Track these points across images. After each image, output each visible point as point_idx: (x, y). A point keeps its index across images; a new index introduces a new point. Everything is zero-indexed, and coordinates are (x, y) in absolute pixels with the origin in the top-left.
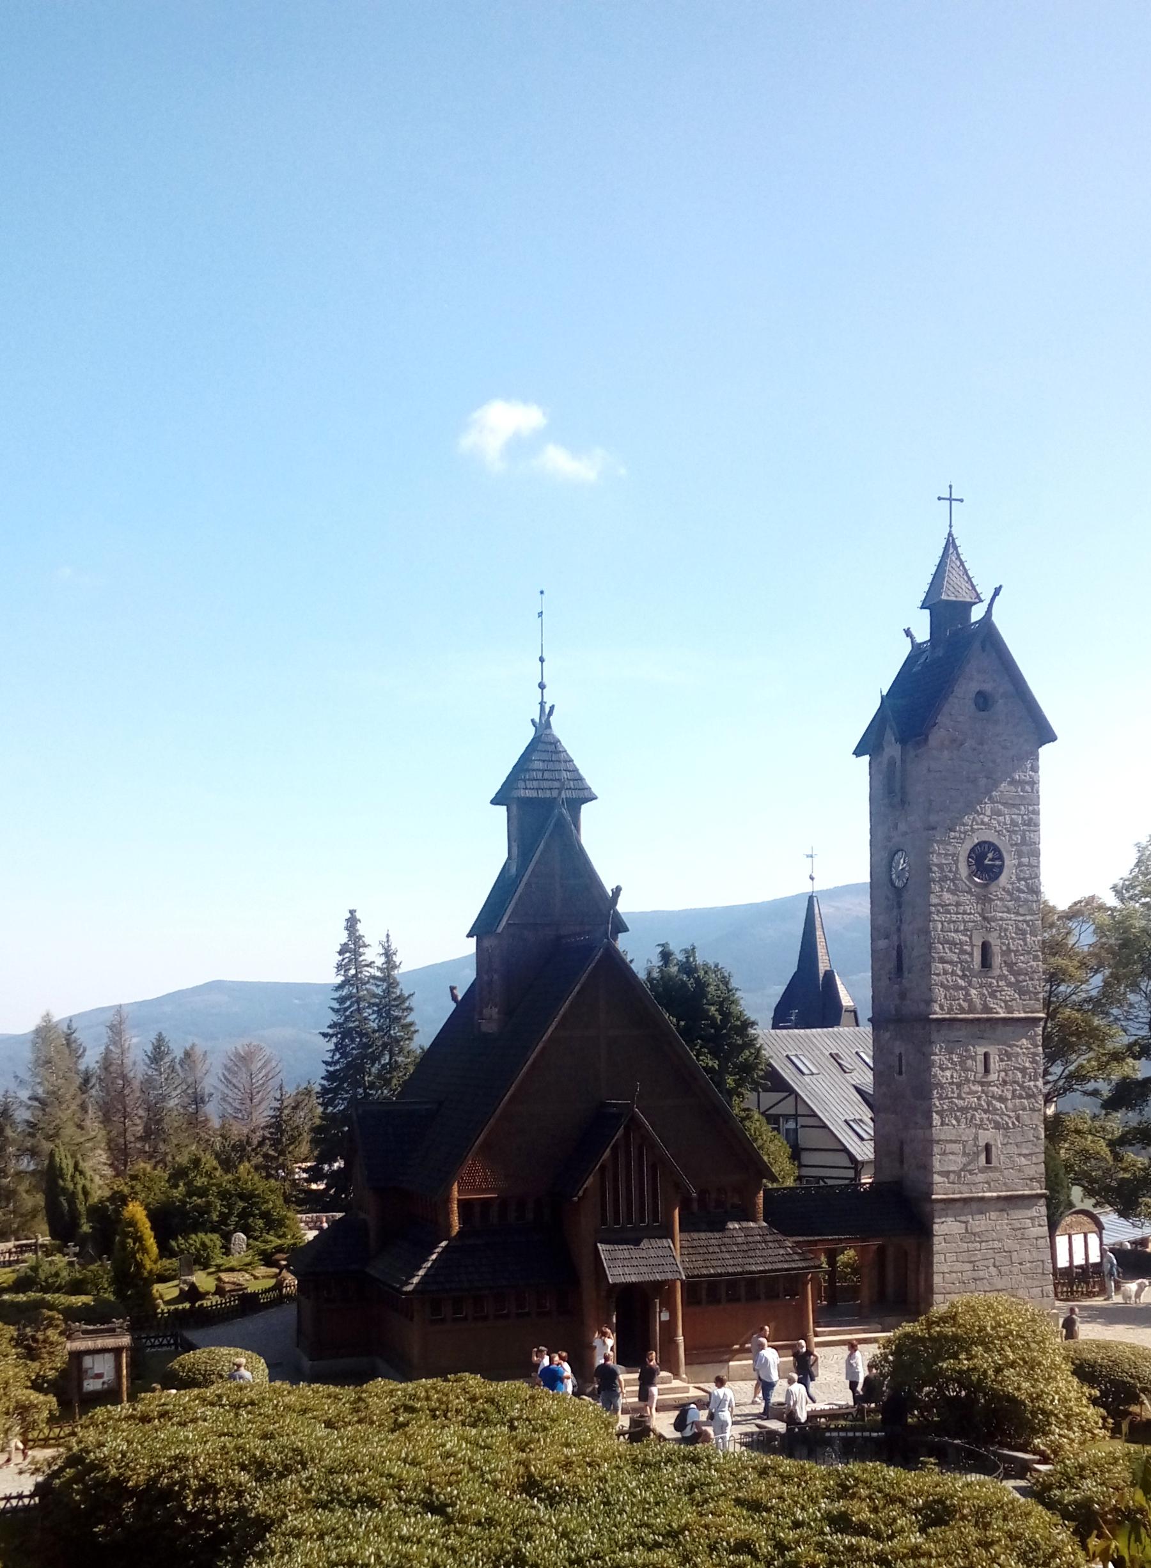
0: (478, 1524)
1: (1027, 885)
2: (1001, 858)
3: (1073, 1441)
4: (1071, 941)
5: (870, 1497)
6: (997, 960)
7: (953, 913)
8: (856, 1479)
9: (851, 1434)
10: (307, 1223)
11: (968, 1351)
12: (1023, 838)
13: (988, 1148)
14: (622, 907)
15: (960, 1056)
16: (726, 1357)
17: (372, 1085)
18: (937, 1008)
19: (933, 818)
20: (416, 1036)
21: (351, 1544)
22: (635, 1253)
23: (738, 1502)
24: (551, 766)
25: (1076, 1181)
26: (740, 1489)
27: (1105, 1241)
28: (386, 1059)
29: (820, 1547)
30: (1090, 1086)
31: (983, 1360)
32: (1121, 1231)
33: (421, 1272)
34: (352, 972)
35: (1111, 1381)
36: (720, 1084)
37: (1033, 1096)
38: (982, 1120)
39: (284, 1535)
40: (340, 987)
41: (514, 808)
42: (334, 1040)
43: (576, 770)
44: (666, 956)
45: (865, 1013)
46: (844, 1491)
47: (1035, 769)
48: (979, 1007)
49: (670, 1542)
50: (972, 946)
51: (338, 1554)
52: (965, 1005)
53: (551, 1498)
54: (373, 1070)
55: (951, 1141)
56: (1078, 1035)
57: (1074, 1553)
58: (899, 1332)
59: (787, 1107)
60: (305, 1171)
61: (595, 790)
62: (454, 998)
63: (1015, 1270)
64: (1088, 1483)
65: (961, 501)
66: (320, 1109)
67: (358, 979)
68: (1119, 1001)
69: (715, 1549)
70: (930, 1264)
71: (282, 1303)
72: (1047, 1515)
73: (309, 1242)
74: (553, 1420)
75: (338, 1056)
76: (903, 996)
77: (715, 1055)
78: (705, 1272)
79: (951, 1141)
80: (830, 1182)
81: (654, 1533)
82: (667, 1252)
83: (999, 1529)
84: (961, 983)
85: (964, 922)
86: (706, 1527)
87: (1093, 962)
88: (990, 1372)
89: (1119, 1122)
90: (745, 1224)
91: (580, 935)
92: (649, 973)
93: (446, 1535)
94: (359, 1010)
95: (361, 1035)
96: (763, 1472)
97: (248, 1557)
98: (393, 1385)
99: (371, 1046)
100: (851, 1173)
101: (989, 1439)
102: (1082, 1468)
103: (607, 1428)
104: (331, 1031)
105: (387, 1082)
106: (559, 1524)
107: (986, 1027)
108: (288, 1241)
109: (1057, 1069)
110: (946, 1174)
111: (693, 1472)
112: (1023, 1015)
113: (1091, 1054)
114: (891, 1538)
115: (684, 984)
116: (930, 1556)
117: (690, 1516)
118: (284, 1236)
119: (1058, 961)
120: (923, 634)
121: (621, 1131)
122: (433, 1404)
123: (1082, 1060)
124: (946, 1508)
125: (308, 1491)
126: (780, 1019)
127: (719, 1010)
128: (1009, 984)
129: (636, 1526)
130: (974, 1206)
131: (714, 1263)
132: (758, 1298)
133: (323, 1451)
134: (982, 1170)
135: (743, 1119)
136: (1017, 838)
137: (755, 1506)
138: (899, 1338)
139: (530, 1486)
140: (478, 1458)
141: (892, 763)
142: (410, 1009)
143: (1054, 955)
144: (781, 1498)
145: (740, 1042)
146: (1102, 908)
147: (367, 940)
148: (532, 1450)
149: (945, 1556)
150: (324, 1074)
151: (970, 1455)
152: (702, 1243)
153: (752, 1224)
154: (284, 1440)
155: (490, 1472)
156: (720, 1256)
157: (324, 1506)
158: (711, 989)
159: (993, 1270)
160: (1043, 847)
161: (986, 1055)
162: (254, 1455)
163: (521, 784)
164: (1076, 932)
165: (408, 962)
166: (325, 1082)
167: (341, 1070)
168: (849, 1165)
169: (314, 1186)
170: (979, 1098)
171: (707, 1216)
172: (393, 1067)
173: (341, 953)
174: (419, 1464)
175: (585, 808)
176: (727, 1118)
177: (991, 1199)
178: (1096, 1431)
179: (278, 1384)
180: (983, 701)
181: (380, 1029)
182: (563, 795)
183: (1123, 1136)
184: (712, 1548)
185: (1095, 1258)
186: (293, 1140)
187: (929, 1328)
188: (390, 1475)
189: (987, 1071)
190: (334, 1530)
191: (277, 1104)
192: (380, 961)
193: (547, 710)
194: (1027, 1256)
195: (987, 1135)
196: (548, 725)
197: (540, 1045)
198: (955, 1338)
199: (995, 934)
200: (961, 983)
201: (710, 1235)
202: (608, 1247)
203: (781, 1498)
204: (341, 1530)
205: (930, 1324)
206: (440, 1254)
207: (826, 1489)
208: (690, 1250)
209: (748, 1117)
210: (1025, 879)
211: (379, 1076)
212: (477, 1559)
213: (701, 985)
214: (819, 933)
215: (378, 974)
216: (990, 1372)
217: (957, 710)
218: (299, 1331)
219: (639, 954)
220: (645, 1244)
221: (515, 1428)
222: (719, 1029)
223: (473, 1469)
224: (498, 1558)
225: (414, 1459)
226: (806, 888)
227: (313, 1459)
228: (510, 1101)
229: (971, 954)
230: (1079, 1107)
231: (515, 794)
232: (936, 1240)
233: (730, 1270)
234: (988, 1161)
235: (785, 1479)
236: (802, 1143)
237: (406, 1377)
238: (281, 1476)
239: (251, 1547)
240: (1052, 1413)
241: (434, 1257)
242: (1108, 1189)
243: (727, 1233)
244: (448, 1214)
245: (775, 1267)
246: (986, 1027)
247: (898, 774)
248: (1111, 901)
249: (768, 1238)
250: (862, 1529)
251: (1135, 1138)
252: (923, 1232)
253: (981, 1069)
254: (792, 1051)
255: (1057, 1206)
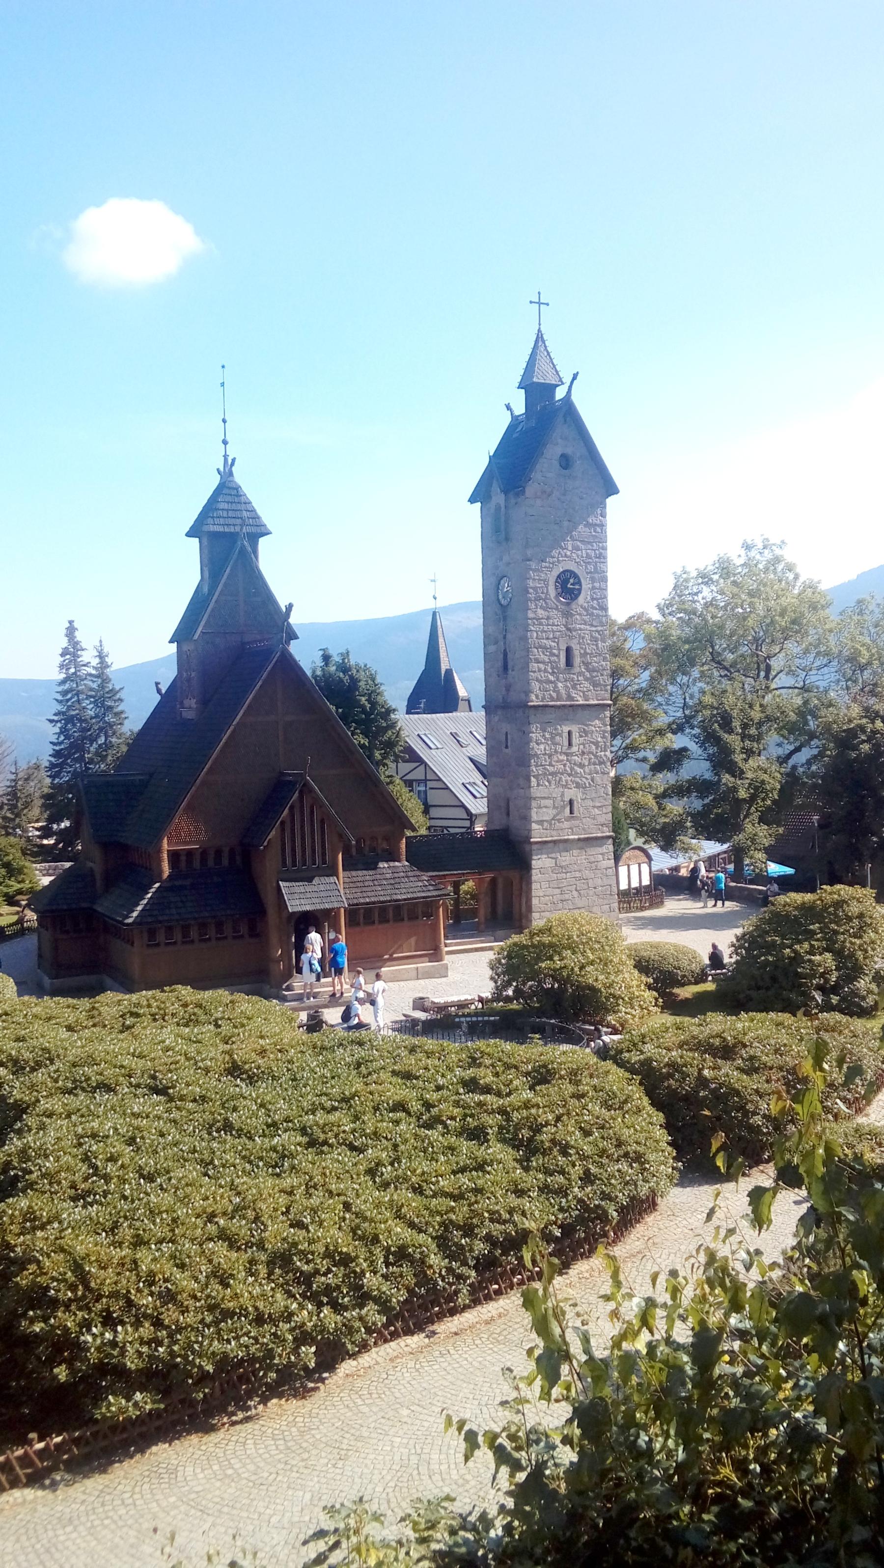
0: (195, 1101)
1: (599, 604)
2: (579, 583)
3: (634, 1016)
4: (627, 645)
5: (492, 1065)
6: (577, 660)
7: (544, 624)
8: (482, 1052)
9: (474, 1019)
10: (41, 871)
11: (559, 954)
12: (595, 568)
13: (571, 802)
14: (292, 620)
15: (552, 733)
16: (379, 964)
17: (91, 761)
18: (533, 697)
19: (529, 552)
20: (126, 722)
21: (93, 1121)
22: (309, 888)
23: (394, 1073)
24: (234, 506)
25: (632, 825)
26: (395, 1063)
27: (653, 869)
28: (102, 740)
29: (457, 1104)
30: (641, 754)
31: (571, 960)
32: (663, 861)
33: (139, 908)
34: (72, 670)
35: (660, 972)
36: (371, 757)
37: (603, 763)
38: (567, 781)
39: (38, 1115)
40: (63, 682)
41: (205, 541)
42: (59, 725)
43: (254, 511)
44: (326, 658)
45: (479, 700)
46: (474, 1062)
47: (603, 515)
48: (564, 696)
49: (344, 1105)
50: (559, 650)
51: (83, 1129)
52: (554, 695)
53: (250, 1078)
54: (92, 749)
55: (544, 798)
56: (633, 717)
57: (640, 1098)
58: (509, 942)
59: (419, 774)
60: (37, 829)
61: (270, 527)
62: (159, 691)
63: (591, 893)
64: (648, 1047)
65: (547, 304)
66: (48, 781)
67: (77, 676)
68: (661, 691)
69: (378, 1109)
70: (529, 890)
71: (23, 934)
72: (621, 1072)
73: (45, 888)
74: (249, 1019)
75: (62, 738)
76: (508, 688)
77: (366, 734)
78: (362, 901)
79: (544, 798)
80: (452, 831)
81: (331, 1100)
82: (333, 887)
83: (587, 1084)
84: (551, 678)
85: (553, 631)
86: (371, 1093)
87: (643, 662)
88: (576, 969)
89: (663, 780)
90: (392, 864)
91: (260, 641)
92: (314, 672)
93: (169, 1111)
94: (79, 701)
95: (81, 721)
96: (412, 1050)
97: (9, 1133)
98: (120, 996)
99: (89, 730)
100: (467, 824)
101: (575, 1017)
102: (644, 1036)
103: (290, 1022)
104: (56, 718)
105: (103, 758)
106: (258, 1098)
107: (571, 711)
108: (27, 885)
109: (617, 742)
110: (540, 822)
111: (360, 1053)
112: (596, 702)
113: (641, 731)
114: (509, 1094)
115: (341, 680)
116: (538, 1107)
117: (358, 1086)
118: (23, 881)
119: (619, 661)
120: (520, 408)
121: (297, 794)
122: (154, 1010)
123: (635, 735)
124: (548, 1071)
125: (56, 1081)
126: (412, 708)
127: (369, 700)
128: (586, 679)
129: (317, 1095)
130: (561, 846)
131: (369, 894)
132: (403, 920)
133: (66, 1049)
134: (568, 819)
135: (388, 784)
136: (591, 568)
137: (408, 1076)
138: (510, 947)
139: (234, 1070)
140: (192, 1050)
141: (498, 508)
142: (121, 700)
143: (616, 656)
144: (426, 1068)
145: (384, 725)
146: (649, 621)
147: (84, 645)
148: (233, 1043)
149: (548, 1106)
150: (51, 752)
151: (562, 1030)
152: (359, 879)
153: (397, 864)
154: (35, 1042)
155: (203, 1060)
156: (374, 888)
157: (70, 1092)
158: (362, 684)
159: (575, 894)
160: (610, 575)
161: (570, 733)
162: (10, 1055)
163: (210, 521)
164: (630, 640)
165: (118, 662)
166: (53, 759)
167: (65, 749)
168: (465, 816)
169: (45, 842)
170: (565, 765)
171: (363, 859)
172: (108, 746)
173: (62, 655)
174: (144, 1057)
175: (262, 541)
176: (376, 782)
177: (573, 840)
178: (651, 1008)
179: (26, 998)
180: (566, 462)
181: (96, 716)
182: (244, 530)
183: (665, 791)
184: (376, 1109)
185: (646, 881)
186: (27, 805)
187: (531, 937)
188: (122, 1066)
189: (570, 744)
190: (79, 1110)
191: (13, 777)
192: (95, 662)
193: (230, 462)
194: (599, 882)
195: (569, 794)
196: (231, 474)
197: (232, 728)
198: (551, 945)
199: (575, 641)
200: (551, 678)
201: (365, 872)
202: (287, 884)
203: (426, 1068)
204: (84, 1110)
205: (532, 935)
206: (154, 893)
207: (460, 1060)
208: (349, 885)
209: (391, 782)
210: (597, 599)
211: (97, 754)
212: (194, 1127)
213: (354, 681)
214: (441, 640)
215: (94, 672)
216: (576, 969)
217: (546, 469)
218: (40, 956)
219: (306, 656)
220: (316, 881)
221: (220, 1026)
222: (368, 714)
223: (188, 1059)
224: (211, 1127)
225: (140, 1053)
226: (430, 605)
227: (58, 1056)
228: (207, 773)
229: (558, 656)
230: (633, 771)
231: (205, 528)
232: (534, 872)
233: (382, 899)
234: (571, 812)
235: (429, 1054)
236: (431, 801)
237: (131, 991)
238: (33, 1070)
239: (11, 1127)
240: (620, 997)
241: (149, 895)
242: (654, 830)
243: (378, 871)
244: (160, 861)
245: (415, 895)
246: (571, 711)
247: (503, 519)
248: (656, 616)
249: (410, 874)
250: (487, 1090)
251: (673, 792)
252: (524, 866)
253: (566, 743)
254: (414, 728)
255: (619, 845)
